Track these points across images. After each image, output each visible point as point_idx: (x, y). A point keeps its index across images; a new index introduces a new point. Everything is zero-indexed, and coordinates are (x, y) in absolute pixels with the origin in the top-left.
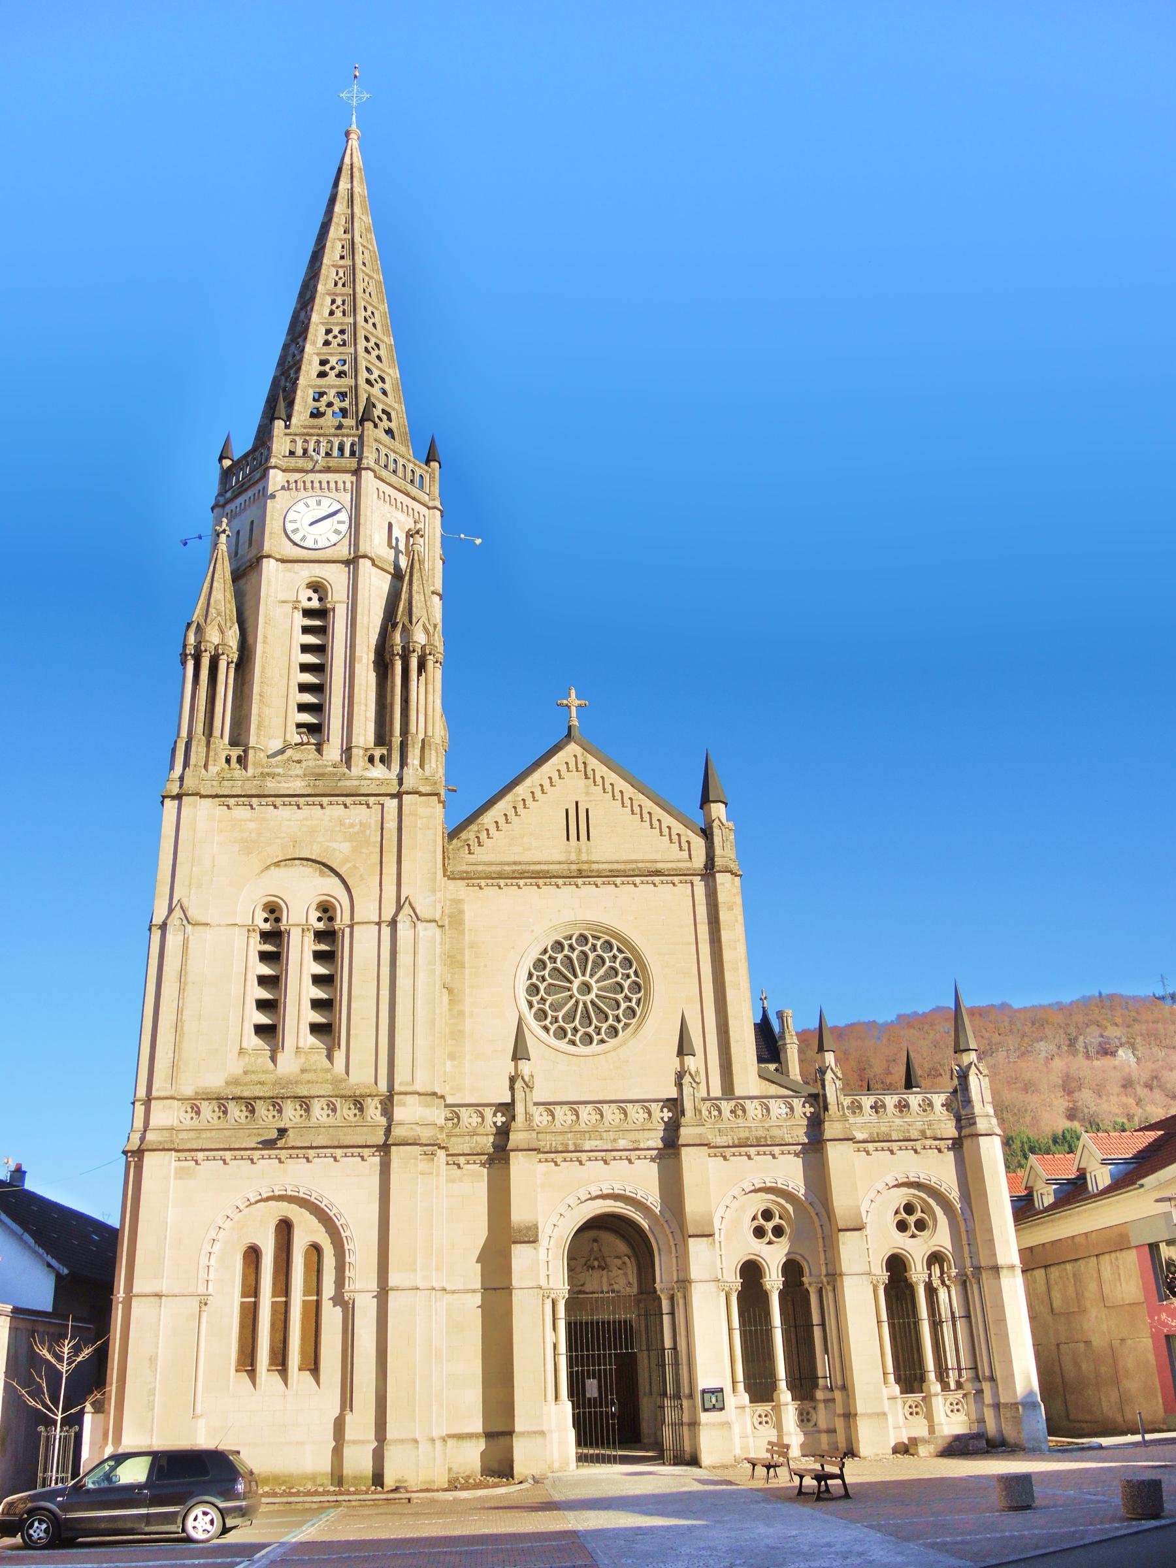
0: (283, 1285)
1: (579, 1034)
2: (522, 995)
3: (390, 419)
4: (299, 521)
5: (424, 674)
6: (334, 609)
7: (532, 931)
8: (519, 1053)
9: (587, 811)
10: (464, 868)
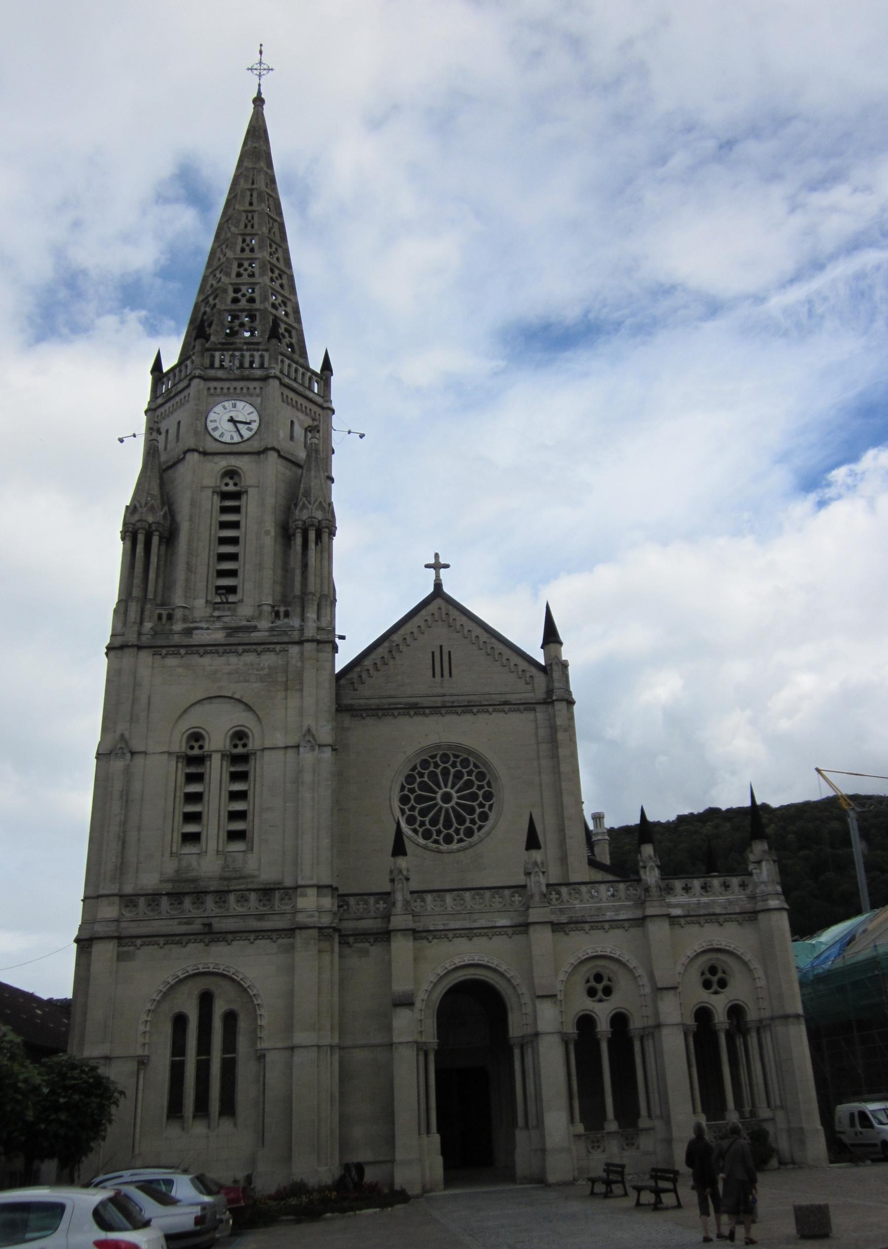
0: (204, 1046)
1: (442, 835)
2: (396, 804)
3: (290, 337)
4: (218, 421)
5: (319, 544)
6: (246, 492)
7: (405, 752)
8: (399, 849)
9: (450, 653)
10: (350, 702)
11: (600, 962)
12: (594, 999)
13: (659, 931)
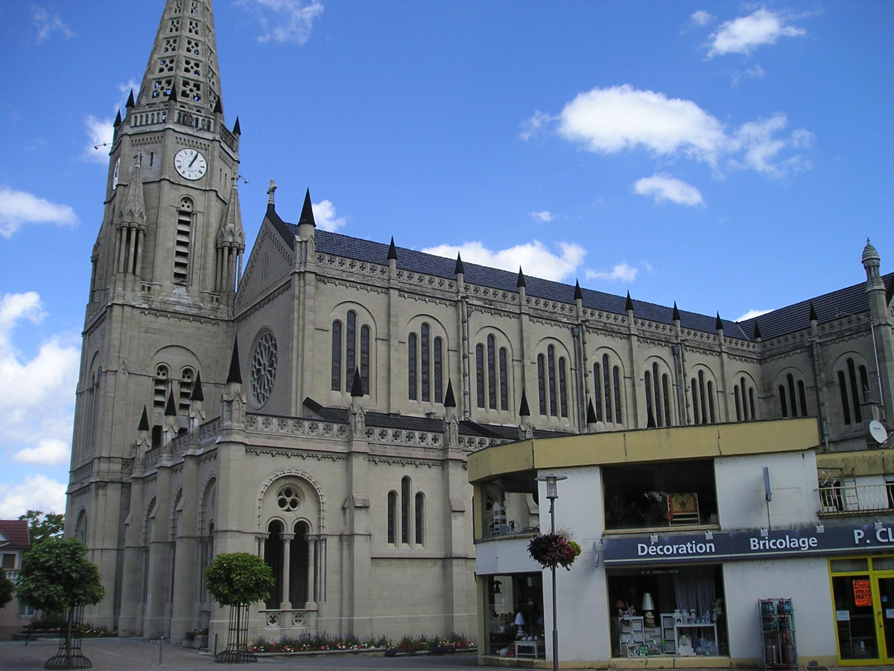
11: (292, 481)
12: (283, 509)
13: (359, 464)
